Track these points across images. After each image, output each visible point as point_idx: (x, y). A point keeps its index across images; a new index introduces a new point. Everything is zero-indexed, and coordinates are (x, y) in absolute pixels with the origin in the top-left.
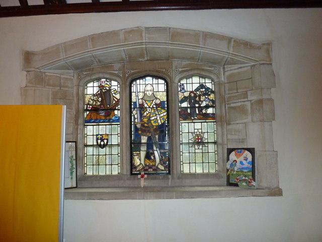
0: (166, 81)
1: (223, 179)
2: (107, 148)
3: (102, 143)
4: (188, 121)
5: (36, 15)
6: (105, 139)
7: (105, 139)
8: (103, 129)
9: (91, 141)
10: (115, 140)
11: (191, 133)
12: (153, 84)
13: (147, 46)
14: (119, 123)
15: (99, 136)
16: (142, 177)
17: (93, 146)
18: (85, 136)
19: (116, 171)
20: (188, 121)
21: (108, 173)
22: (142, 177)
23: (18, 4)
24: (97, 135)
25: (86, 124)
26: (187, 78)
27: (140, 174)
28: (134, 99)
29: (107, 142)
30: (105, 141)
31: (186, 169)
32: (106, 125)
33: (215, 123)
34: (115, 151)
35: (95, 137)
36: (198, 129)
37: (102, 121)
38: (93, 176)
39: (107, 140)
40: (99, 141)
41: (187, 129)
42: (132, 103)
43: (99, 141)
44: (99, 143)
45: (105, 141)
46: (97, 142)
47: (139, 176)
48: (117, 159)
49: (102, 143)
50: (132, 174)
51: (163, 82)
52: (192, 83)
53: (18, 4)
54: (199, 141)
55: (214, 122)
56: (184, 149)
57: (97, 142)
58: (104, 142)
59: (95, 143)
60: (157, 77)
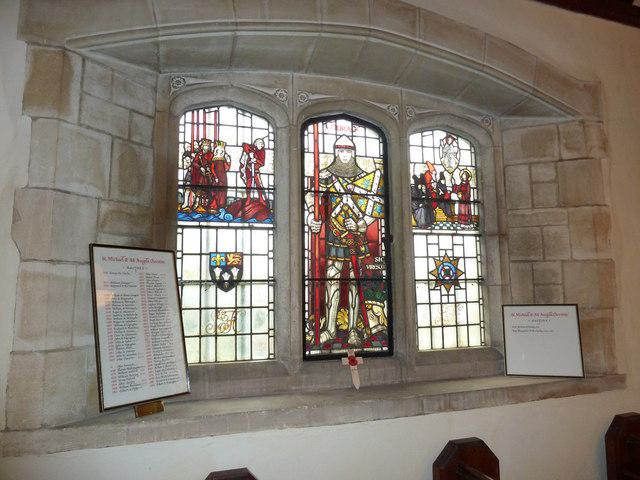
1: (288, 378)
2: (239, 288)
3: (226, 277)
6: (232, 266)
7: (232, 266)
8: (226, 239)
10: (260, 268)
11: (433, 257)
12: (336, 135)
13: (238, 33)
16: (353, 362)
17: (200, 283)
19: (260, 350)
21: (438, 345)
22: (353, 362)
26: (243, 109)
28: (309, 170)
29: (241, 273)
30: (235, 272)
33: (271, 232)
34: (262, 295)
37: (197, 216)
39: (240, 267)
41: (426, 249)
43: (218, 271)
45: (235, 272)
47: (345, 361)
48: (262, 321)
49: (226, 277)
54: (447, 276)
56: (422, 292)
57: (212, 273)
58: (231, 274)
59: (206, 276)
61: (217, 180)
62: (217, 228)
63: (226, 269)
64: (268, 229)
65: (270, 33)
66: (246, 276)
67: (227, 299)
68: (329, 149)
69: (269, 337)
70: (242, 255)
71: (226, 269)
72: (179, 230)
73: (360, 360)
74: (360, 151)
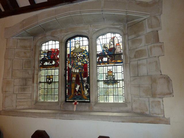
0: (88, 39)
3: (49, 81)
4: (45, 69)
5: (3, 17)
7: (51, 78)
9: (43, 79)
14: (122, 64)
15: (48, 77)
17: (44, 82)
18: (39, 76)
20: (45, 69)
22: (76, 104)
23: (29, 4)
24: (47, 76)
25: (98, 66)
27: (74, 102)
29: (52, 80)
30: (51, 80)
31: (101, 102)
32: (45, 70)
33: (122, 66)
34: (121, 84)
35: (46, 77)
36: (110, 69)
38: (114, 103)
39: (52, 79)
40: (48, 80)
42: (67, 55)
43: (48, 80)
44: (48, 81)
45: (51, 80)
46: (47, 80)
47: (74, 103)
49: (49, 81)
50: (66, 101)
51: (86, 39)
52: (106, 38)
53: (29, 4)
55: (121, 65)
56: (101, 85)
57: (47, 80)
58: (50, 80)
59: (46, 81)
60: (83, 36)
61: (58, 56)
62: (117, 65)
63: (49, 79)
64: (121, 65)
65: (106, 13)
66: (54, 81)
67: (50, 86)
68: (73, 46)
69: (123, 89)
70: (53, 76)
71: (49, 79)
72: (98, 67)
73: (78, 103)
74: (81, 45)
